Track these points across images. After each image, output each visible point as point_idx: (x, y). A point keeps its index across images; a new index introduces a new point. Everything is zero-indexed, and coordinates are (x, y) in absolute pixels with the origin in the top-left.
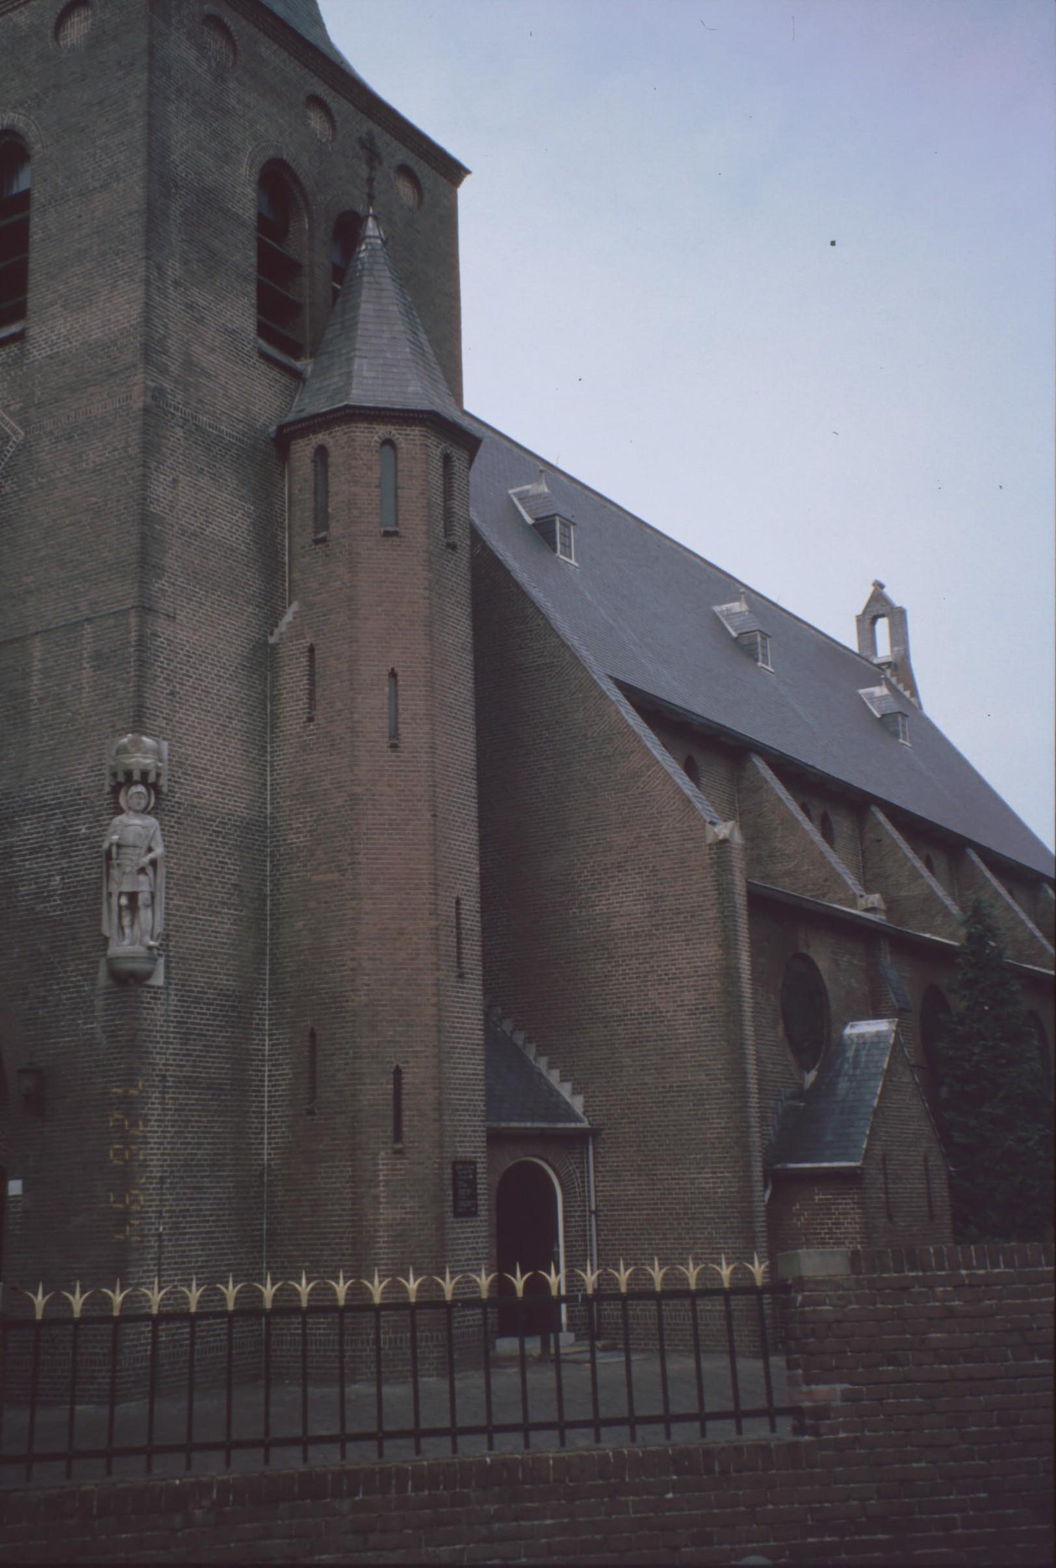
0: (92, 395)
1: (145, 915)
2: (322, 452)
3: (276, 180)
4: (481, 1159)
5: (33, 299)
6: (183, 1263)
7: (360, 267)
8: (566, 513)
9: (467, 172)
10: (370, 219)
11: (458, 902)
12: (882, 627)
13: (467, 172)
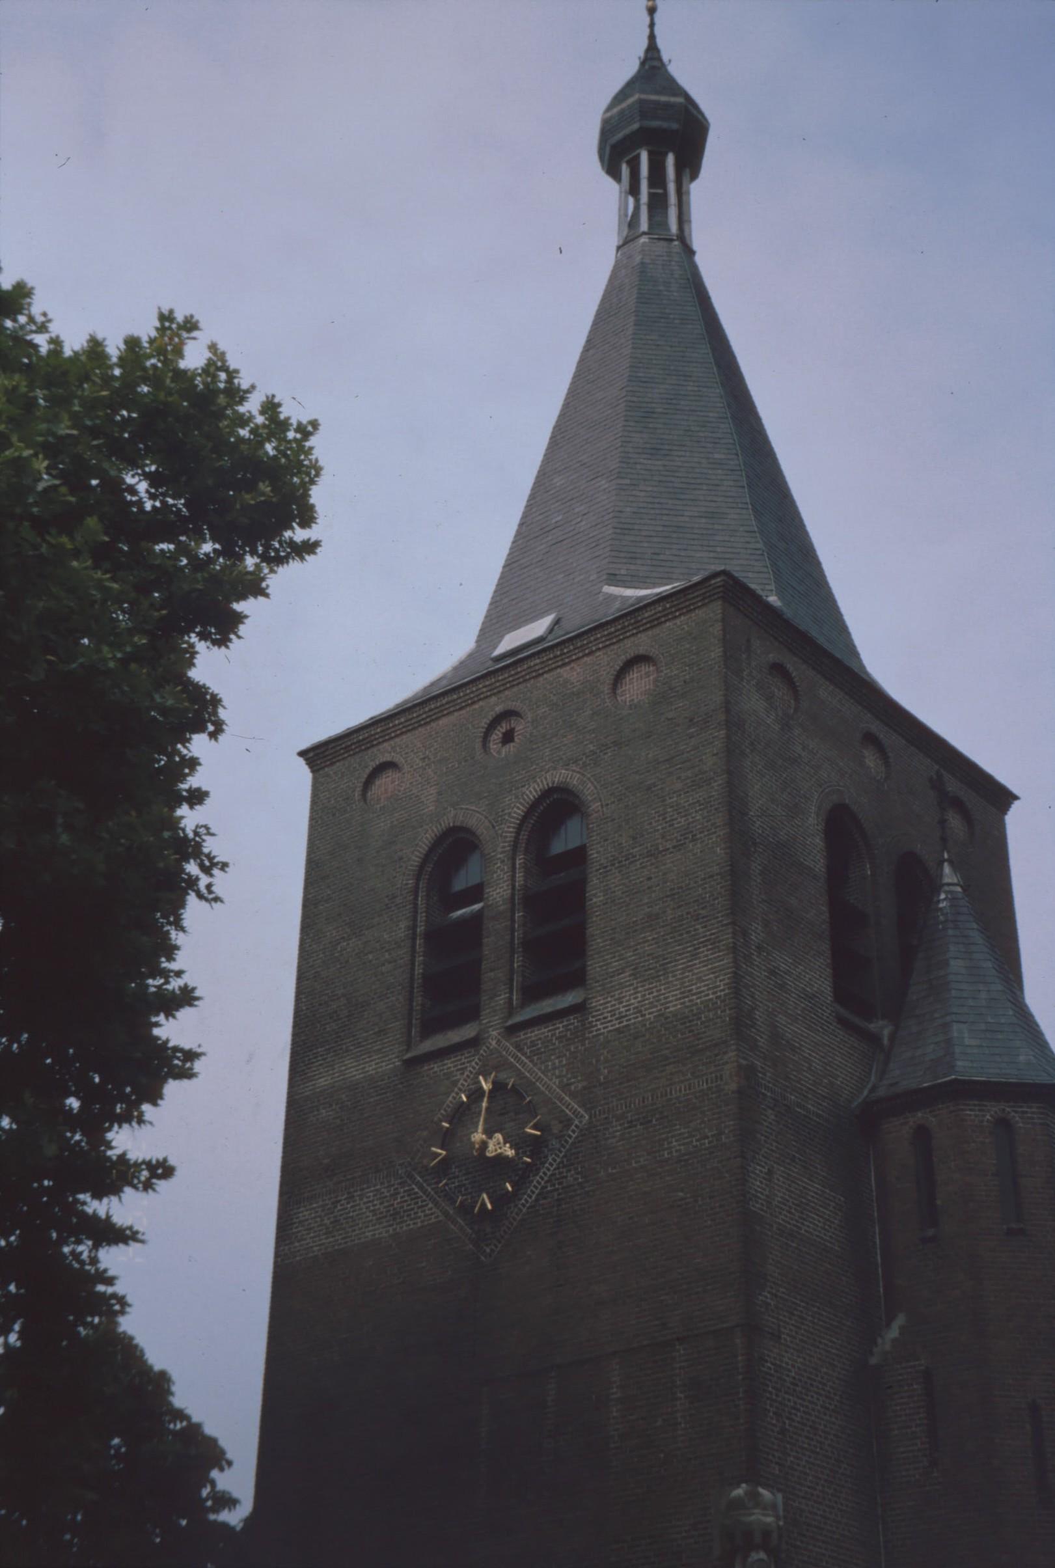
0: (671, 1074)
2: (922, 1134)
3: (841, 825)
5: (594, 967)
7: (942, 918)
9: (1016, 798)
10: (946, 864)
13: (1016, 798)
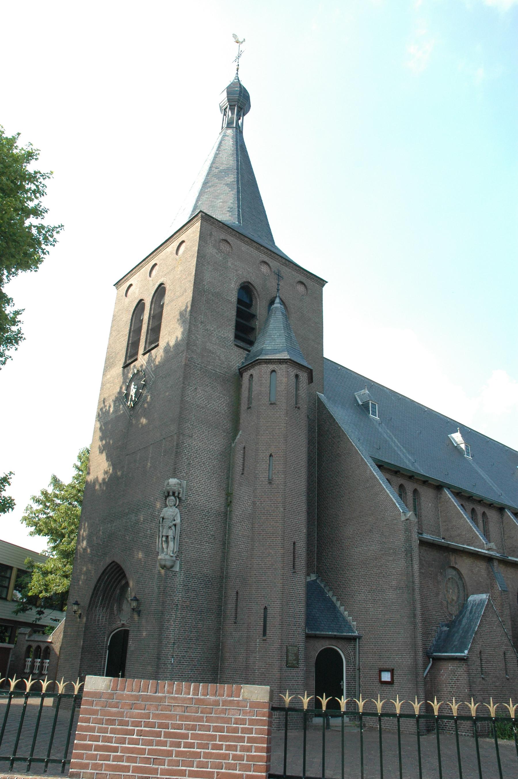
1: (171, 544)
3: (246, 290)
4: (302, 645)
6: (182, 676)
11: (294, 543)
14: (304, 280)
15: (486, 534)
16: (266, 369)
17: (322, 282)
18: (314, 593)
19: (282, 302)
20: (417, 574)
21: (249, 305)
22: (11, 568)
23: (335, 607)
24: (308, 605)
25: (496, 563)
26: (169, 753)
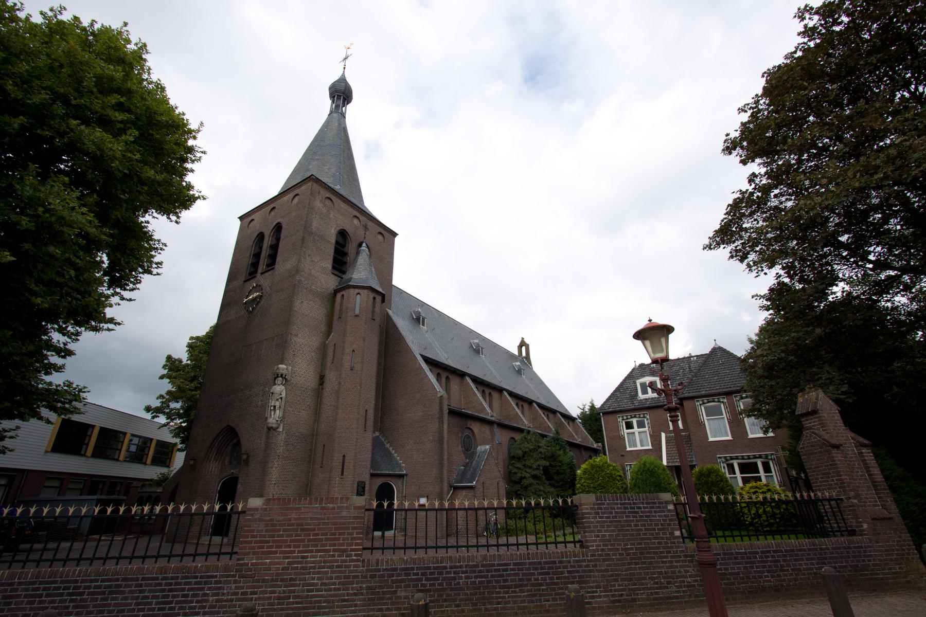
1: (278, 412)
3: (342, 234)
8: (421, 315)
12: (524, 348)
14: (383, 231)
15: (491, 406)
16: (353, 292)
17: (394, 234)
18: (377, 445)
19: (368, 247)
20: (446, 432)
21: (344, 246)
22: (93, 426)
23: (391, 454)
24: (373, 454)
25: (495, 426)
26: (303, 541)
